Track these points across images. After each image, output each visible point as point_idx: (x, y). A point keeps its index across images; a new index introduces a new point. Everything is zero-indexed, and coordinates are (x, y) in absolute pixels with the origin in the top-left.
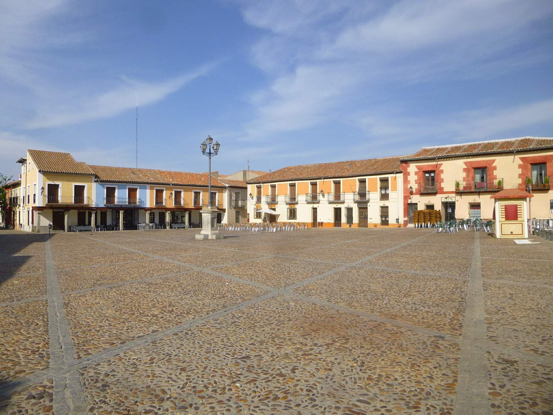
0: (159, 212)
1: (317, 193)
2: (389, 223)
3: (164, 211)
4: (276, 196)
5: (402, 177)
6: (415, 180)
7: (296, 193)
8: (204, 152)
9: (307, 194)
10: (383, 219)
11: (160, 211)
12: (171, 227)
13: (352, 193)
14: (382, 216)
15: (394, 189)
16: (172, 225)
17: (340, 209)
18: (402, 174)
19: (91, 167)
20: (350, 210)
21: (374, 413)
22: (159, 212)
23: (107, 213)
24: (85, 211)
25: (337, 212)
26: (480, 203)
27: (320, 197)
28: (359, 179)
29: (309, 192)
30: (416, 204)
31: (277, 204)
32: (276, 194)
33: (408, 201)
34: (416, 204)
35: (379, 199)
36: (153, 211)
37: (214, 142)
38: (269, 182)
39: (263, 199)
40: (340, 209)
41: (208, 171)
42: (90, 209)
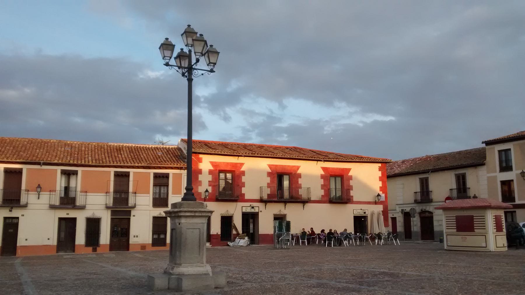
6: (209, 181)
7: (23, 187)
30: (18, 218)
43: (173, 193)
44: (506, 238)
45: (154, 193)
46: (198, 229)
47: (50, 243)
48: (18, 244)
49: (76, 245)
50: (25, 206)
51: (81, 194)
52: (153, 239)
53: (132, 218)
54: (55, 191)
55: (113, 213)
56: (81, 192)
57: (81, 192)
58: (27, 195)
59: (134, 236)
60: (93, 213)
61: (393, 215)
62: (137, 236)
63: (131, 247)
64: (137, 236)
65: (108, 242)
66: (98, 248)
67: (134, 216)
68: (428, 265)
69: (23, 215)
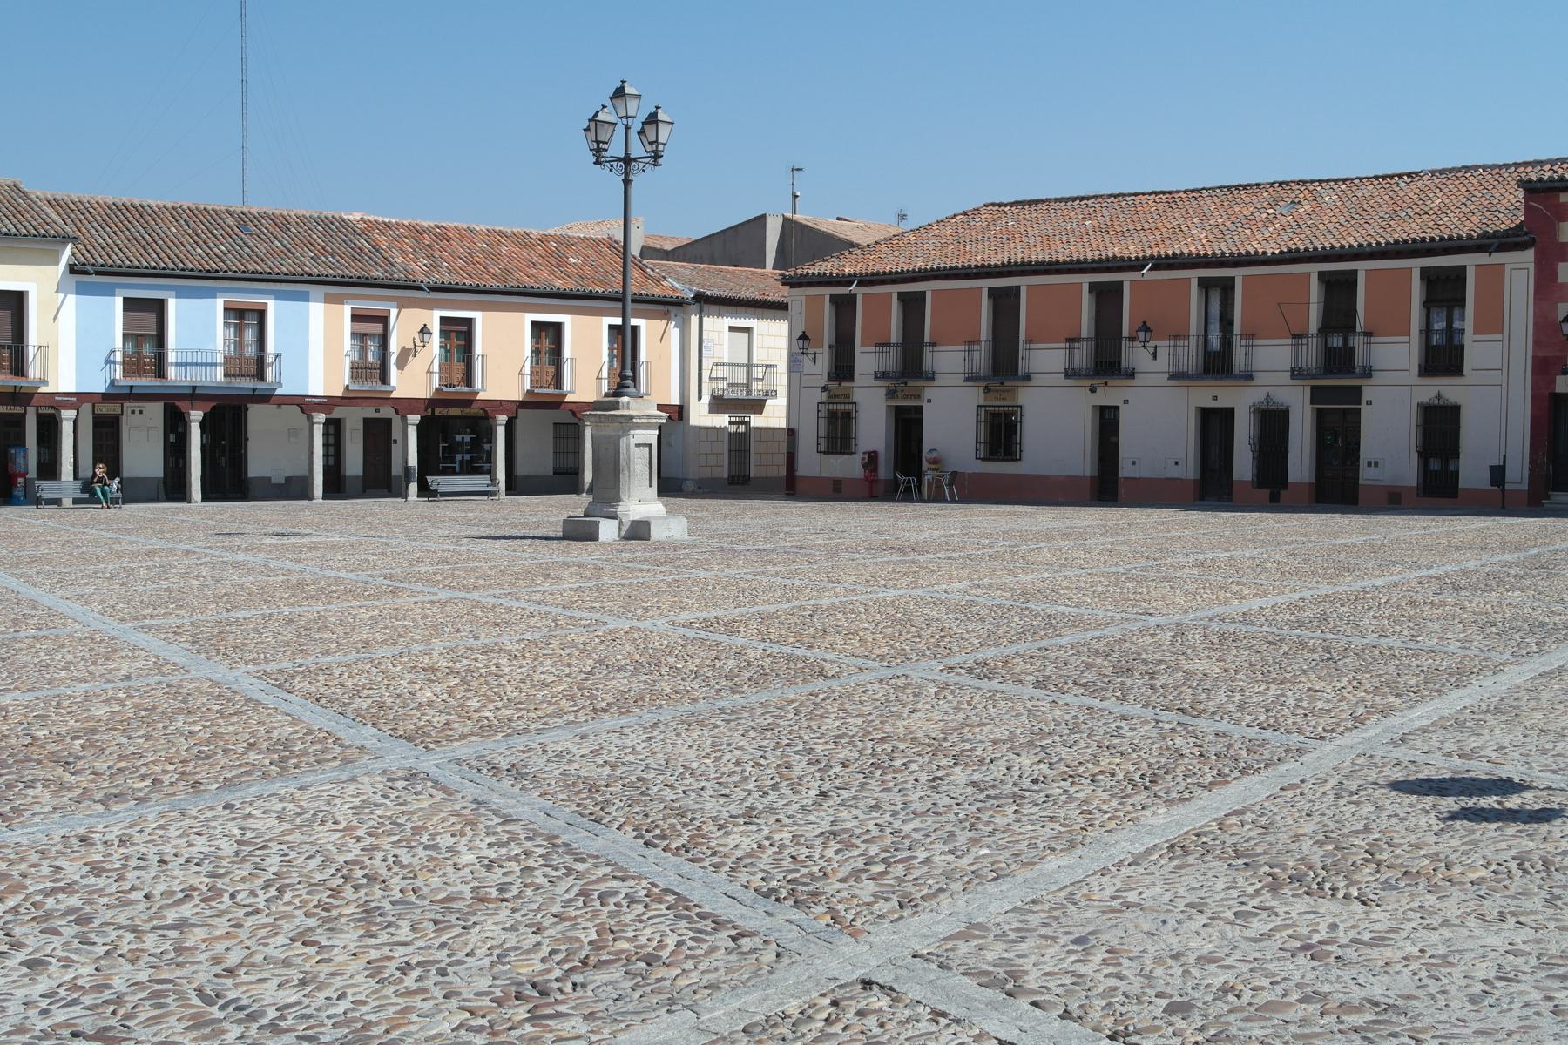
0: (367, 421)
1: (1120, 338)
2: (1461, 485)
3: (387, 412)
4: (927, 349)
5: (1532, 267)
7: (1022, 335)
8: (598, 152)
9: (1071, 340)
10: (1435, 465)
11: (370, 413)
12: (424, 490)
13: (1289, 341)
14: (1425, 453)
15: (1491, 323)
16: (429, 479)
17: (1228, 414)
18: (1529, 255)
19: (54, 203)
20: (1273, 422)
21: (619, 85)
22: (367, 421)
23: (124, 418)
24: (20, 410)
25: (1215, 424)
26: (1094, 407)
27: (1136, 355)
28: (1321, 275)
29: (1084, 334)
30: (1117, 408)
31: (931, 378)
32: (927, 339)
33: (1554, 381)
34: (1117, 408)
35: (1415, 370)
36: (337, 413)
37: (638, 112)
38: (894, 282)
39: (865, 360)
40: (1228, 414)
41: (705, 319)
42: (578, 410)
43: (863, 345)
44: (1196, 516)
45: (1427, 331)
46: (645, 445)
47: (1175, 473)
48: (1121, 474)
49: (1235, 486)
50: (1131, 375)
51: (1243, 342)
52: (1426, 473)
53: (1364, 408)
54: (978, 342)
55: (1317, 394)
56: (1244, 336)
57: (1244, 336)
58: (755, 362)
59: (1369, 464)
60: (1436, 394)
61: (1215, 398)
62: (1376, 464)
63: (1460, 493)
64: (1376, 464)
65: (360, 472)
66: (1283, 492)
67: (1369, 403)
68: (465, 588)
69: (1126, 402)
